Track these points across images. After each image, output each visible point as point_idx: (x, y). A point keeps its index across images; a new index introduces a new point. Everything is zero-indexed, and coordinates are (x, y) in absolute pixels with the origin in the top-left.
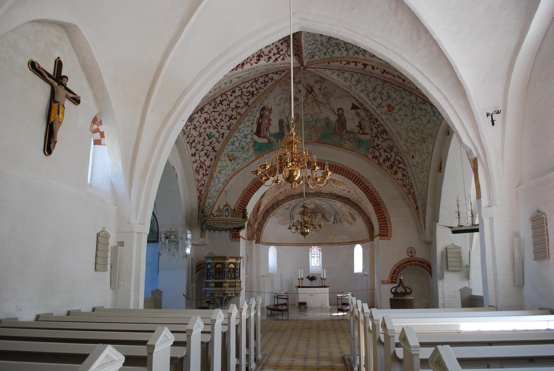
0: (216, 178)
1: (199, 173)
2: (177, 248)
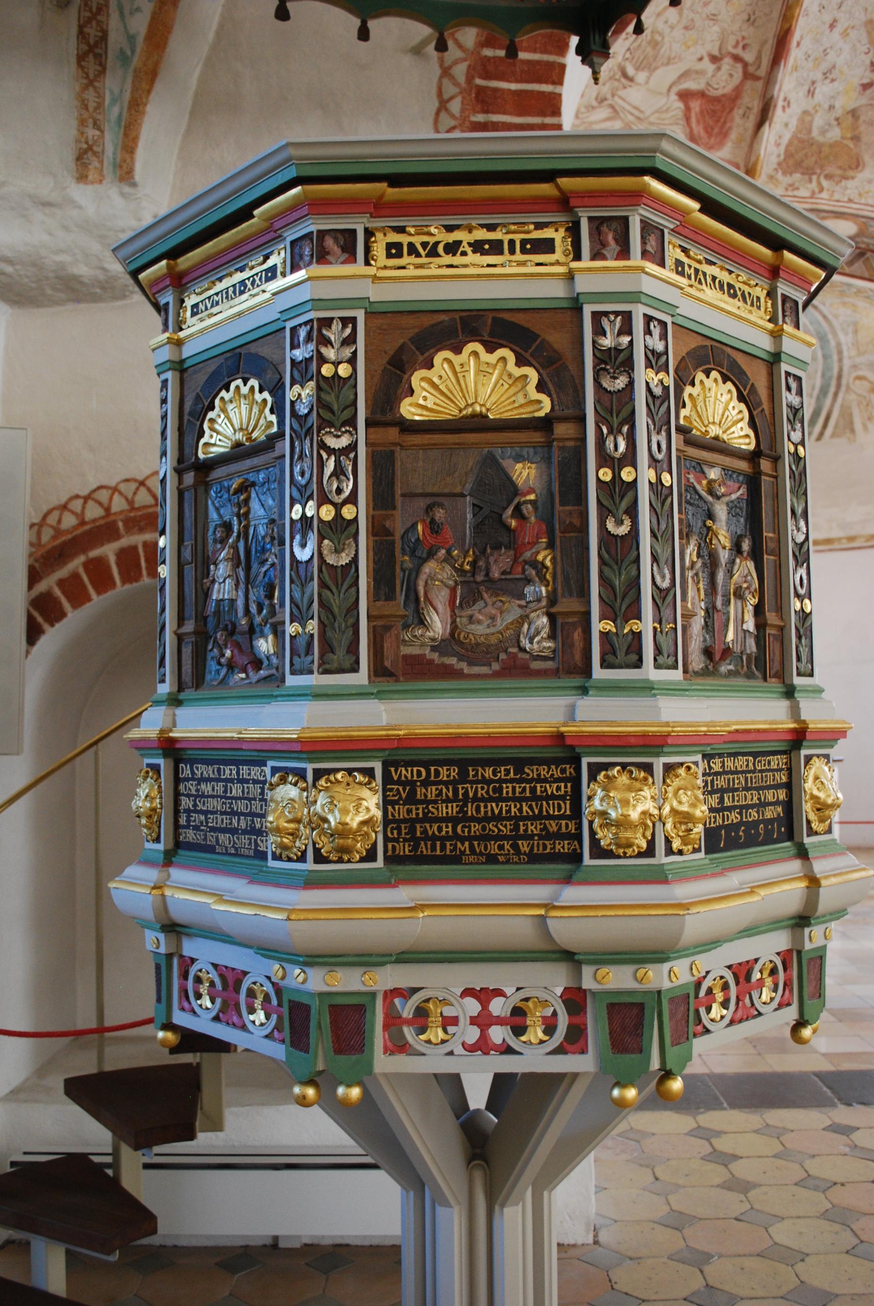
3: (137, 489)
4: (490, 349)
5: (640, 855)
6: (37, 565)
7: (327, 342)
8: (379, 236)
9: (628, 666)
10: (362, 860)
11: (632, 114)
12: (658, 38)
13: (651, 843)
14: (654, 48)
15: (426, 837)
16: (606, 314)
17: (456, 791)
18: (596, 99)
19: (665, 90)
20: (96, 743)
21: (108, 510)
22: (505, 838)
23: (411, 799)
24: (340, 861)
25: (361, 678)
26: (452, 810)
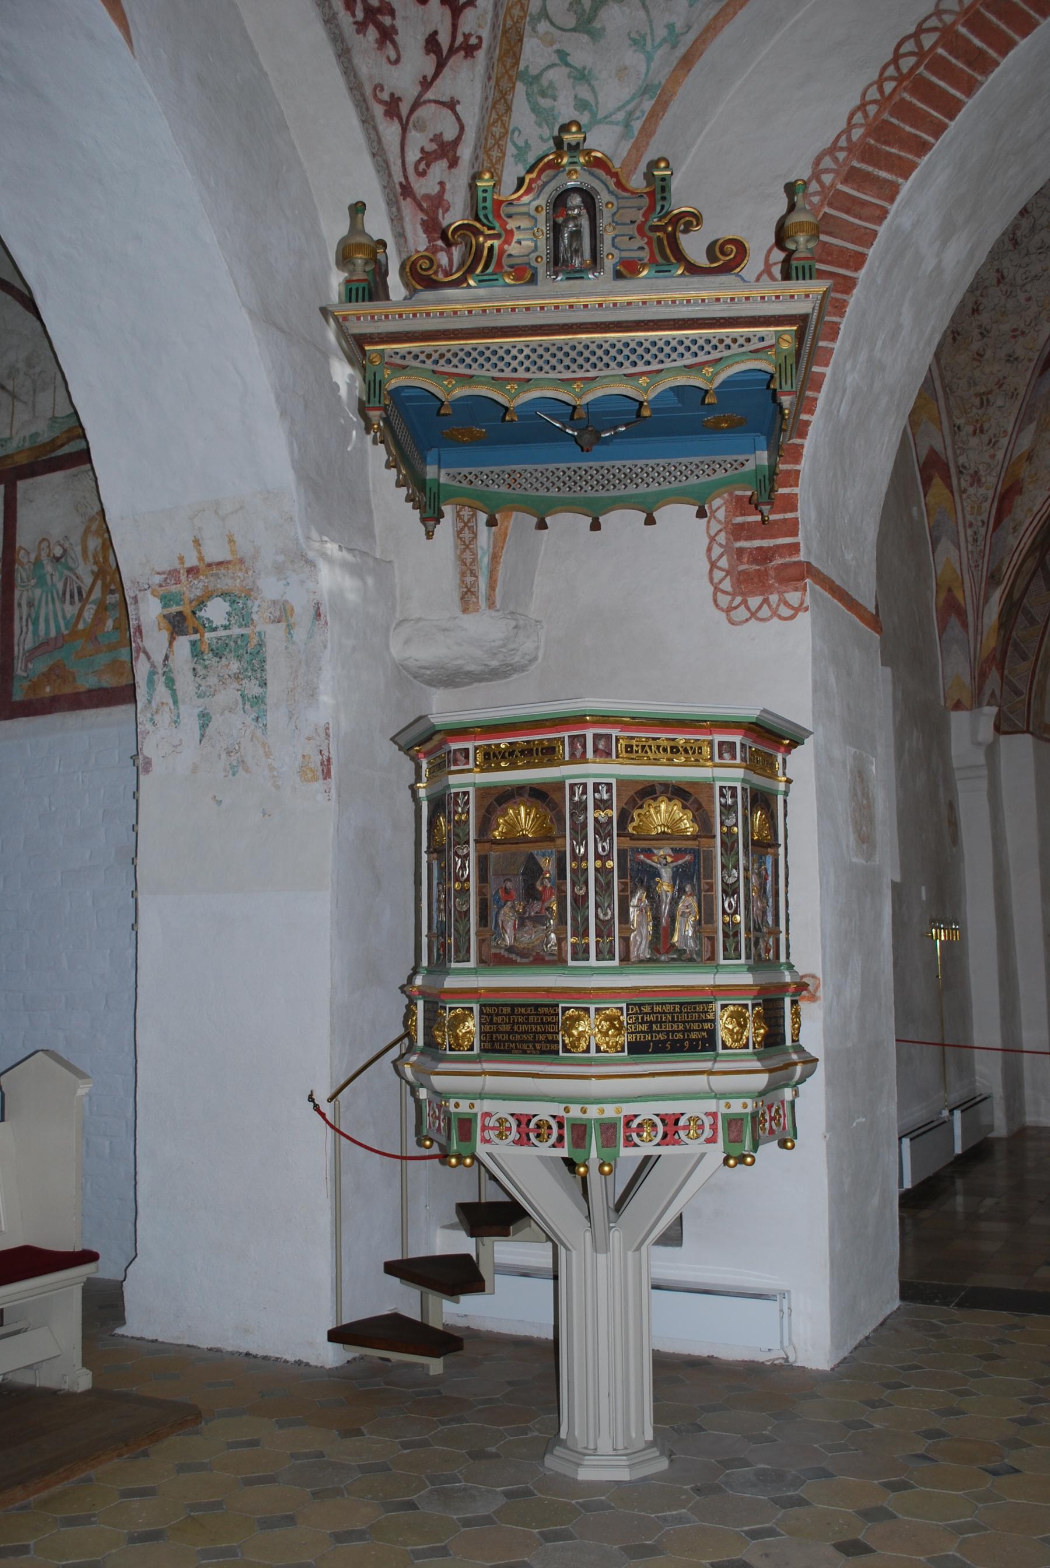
0: (557, 76)
1: (387, 35)
2: (258, 701)
10: (468, 1050)
13: (588, 1047)
22: (530, 1042)
23: (491, 1023)
26: (508, 1028)
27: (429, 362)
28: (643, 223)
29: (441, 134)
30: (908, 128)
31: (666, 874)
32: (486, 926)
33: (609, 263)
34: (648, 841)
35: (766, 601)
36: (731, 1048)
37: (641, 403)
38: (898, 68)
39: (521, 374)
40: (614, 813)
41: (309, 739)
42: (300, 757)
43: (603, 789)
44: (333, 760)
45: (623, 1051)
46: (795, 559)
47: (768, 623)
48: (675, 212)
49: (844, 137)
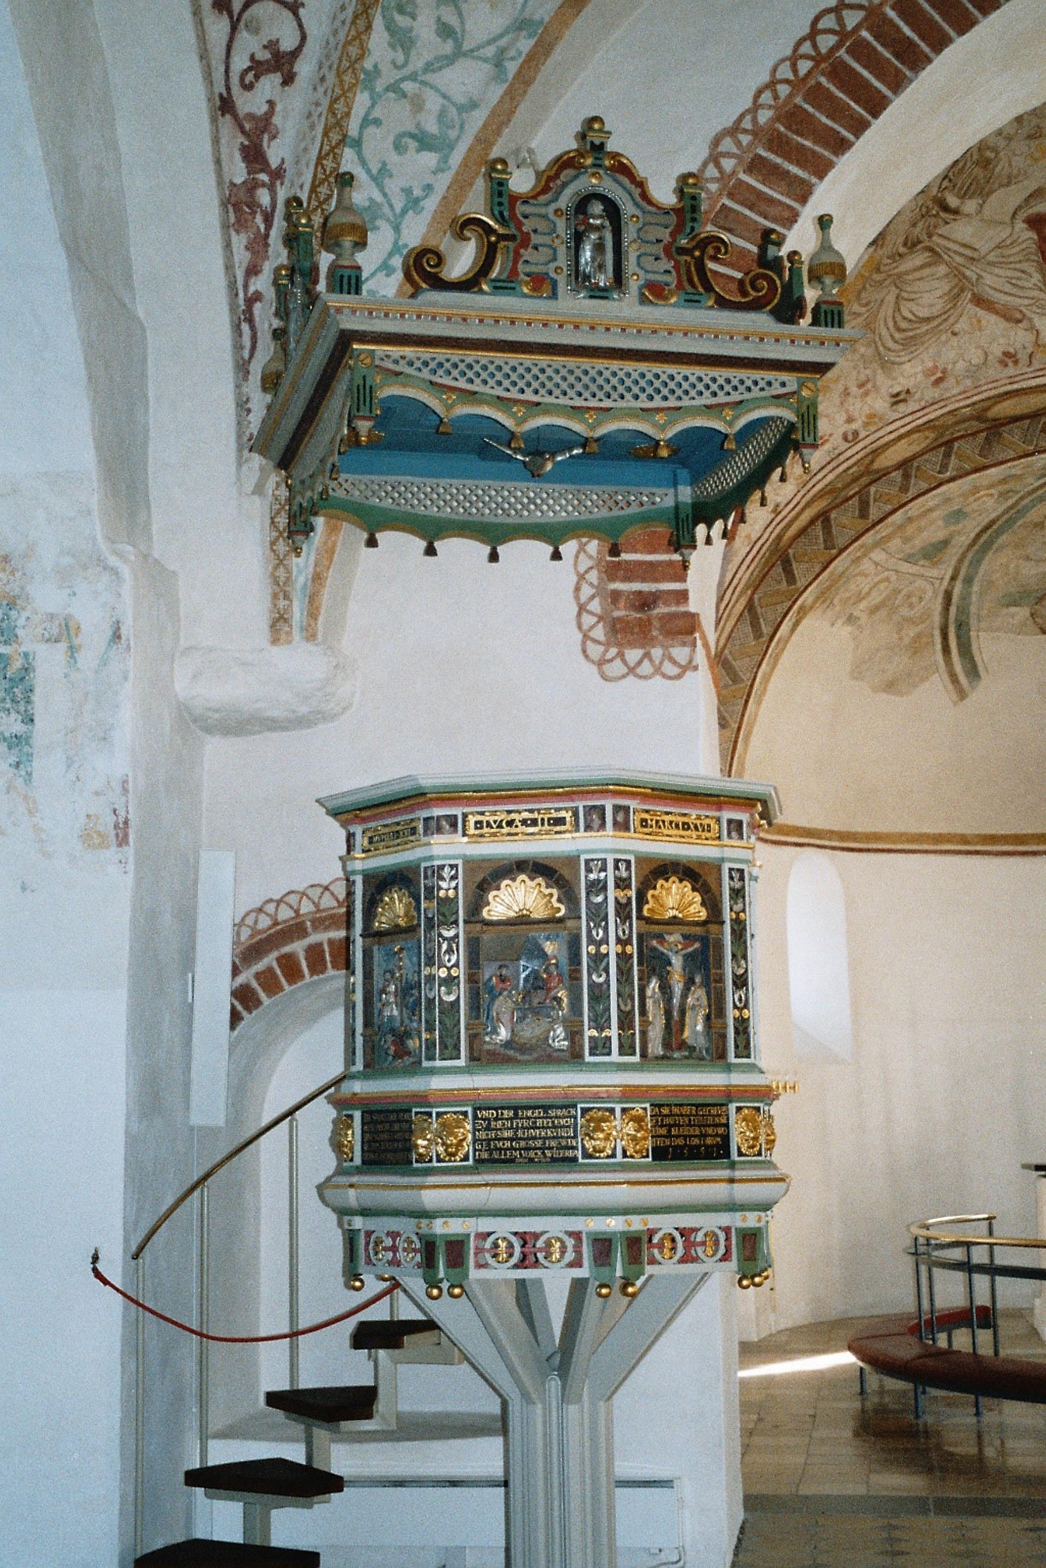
3: (322, 893)
4: (532, 879)
5: (608, 1157)
6: (237, 961)
7: (443, 879)
8: (470, 817)
9: (604, 1055)
10: (461, 1161)
11: (961, 255)
12: (990, 155)
14: (985, 167)
15: (496, 1149)
16: (593, 860)
17: (512, 1123)
18: (905, 244)
19: (1007, 219)
20: (291, 1113)
21: (297, 912)
22: (539, 1149)
23: (488, 1128)
24: (450, 1161)
25: (461, 1062)
27: (425, 371)
28: (670, 244)
29: (278, 41)
30: (824, 119)
31: (677, 962)
32: (478, 1017)
33: (634, 285)
34: (656, 927)
35: (647, 655)
36: (746, 1155)
37: (657, 442)
38: (815, 46)
39: (529, 396)
40: (633, 893)
41: (97, 794)
42: (83, 819)
43: (622, 866)
44: (131, 823)
45: (647, 1156)
46: (682, 609)
47: (650, 681)
48: (702, 236)
49: (748, 117)
